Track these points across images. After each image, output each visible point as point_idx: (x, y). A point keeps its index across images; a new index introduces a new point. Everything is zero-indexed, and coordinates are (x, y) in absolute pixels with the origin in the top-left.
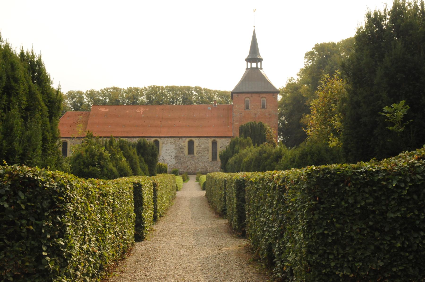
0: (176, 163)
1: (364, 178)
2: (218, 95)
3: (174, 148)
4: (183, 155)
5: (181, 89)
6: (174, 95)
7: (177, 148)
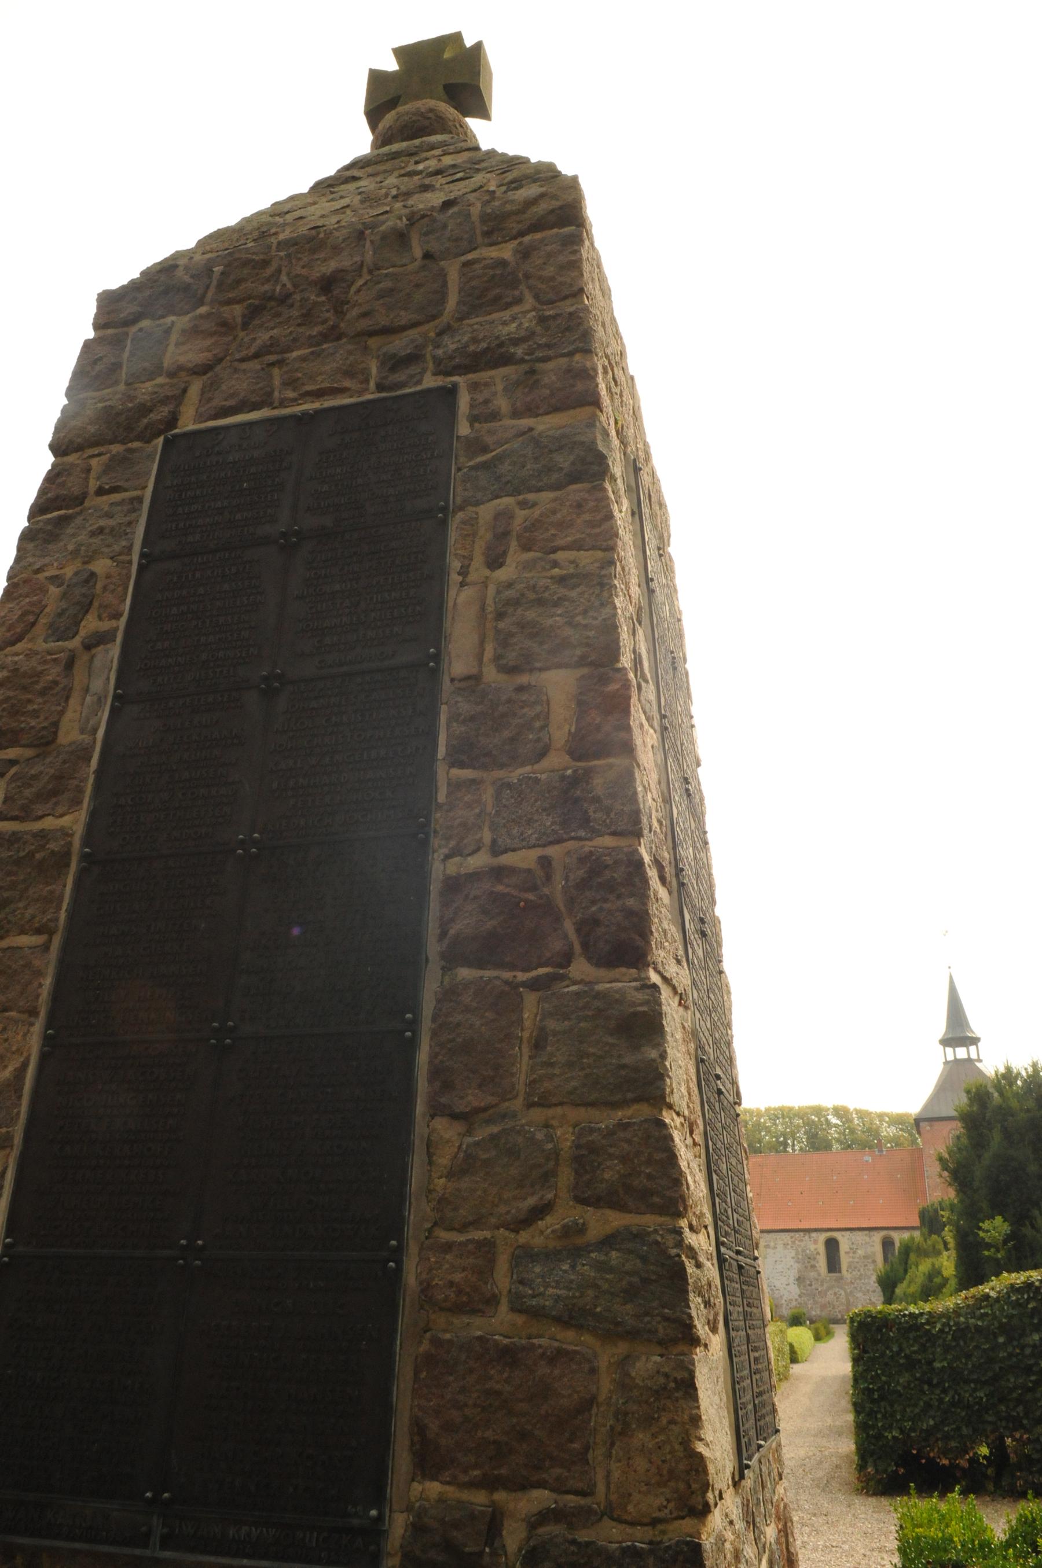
0: (800, 1296)
1: (907, 1322)
2: (890, 1125)
3: (793, 1258)
4: (816, 1276)
5: (802, 1114)
6: (786, 1128)
7: (800, 1257)
